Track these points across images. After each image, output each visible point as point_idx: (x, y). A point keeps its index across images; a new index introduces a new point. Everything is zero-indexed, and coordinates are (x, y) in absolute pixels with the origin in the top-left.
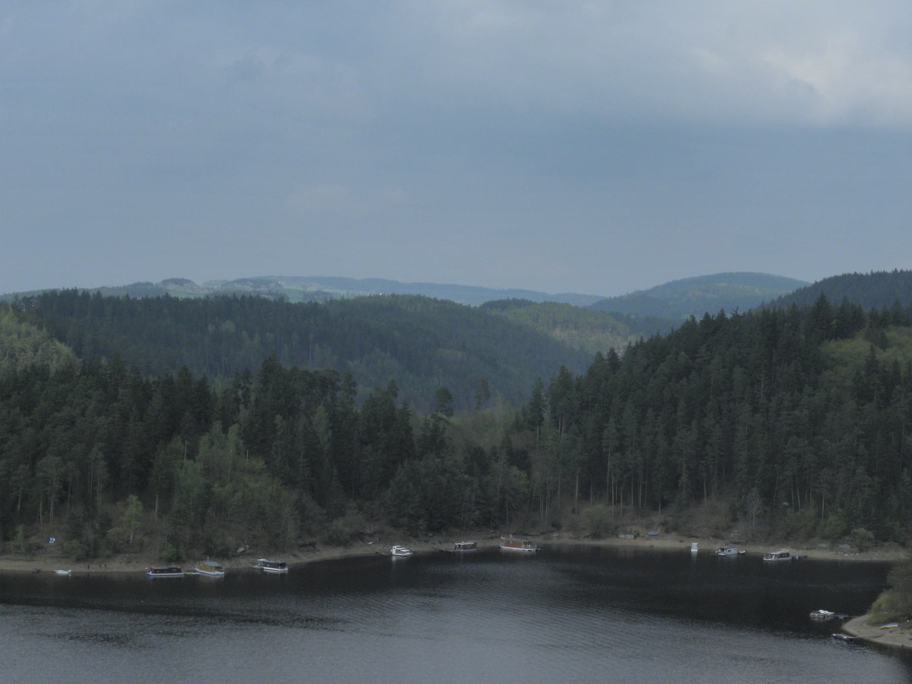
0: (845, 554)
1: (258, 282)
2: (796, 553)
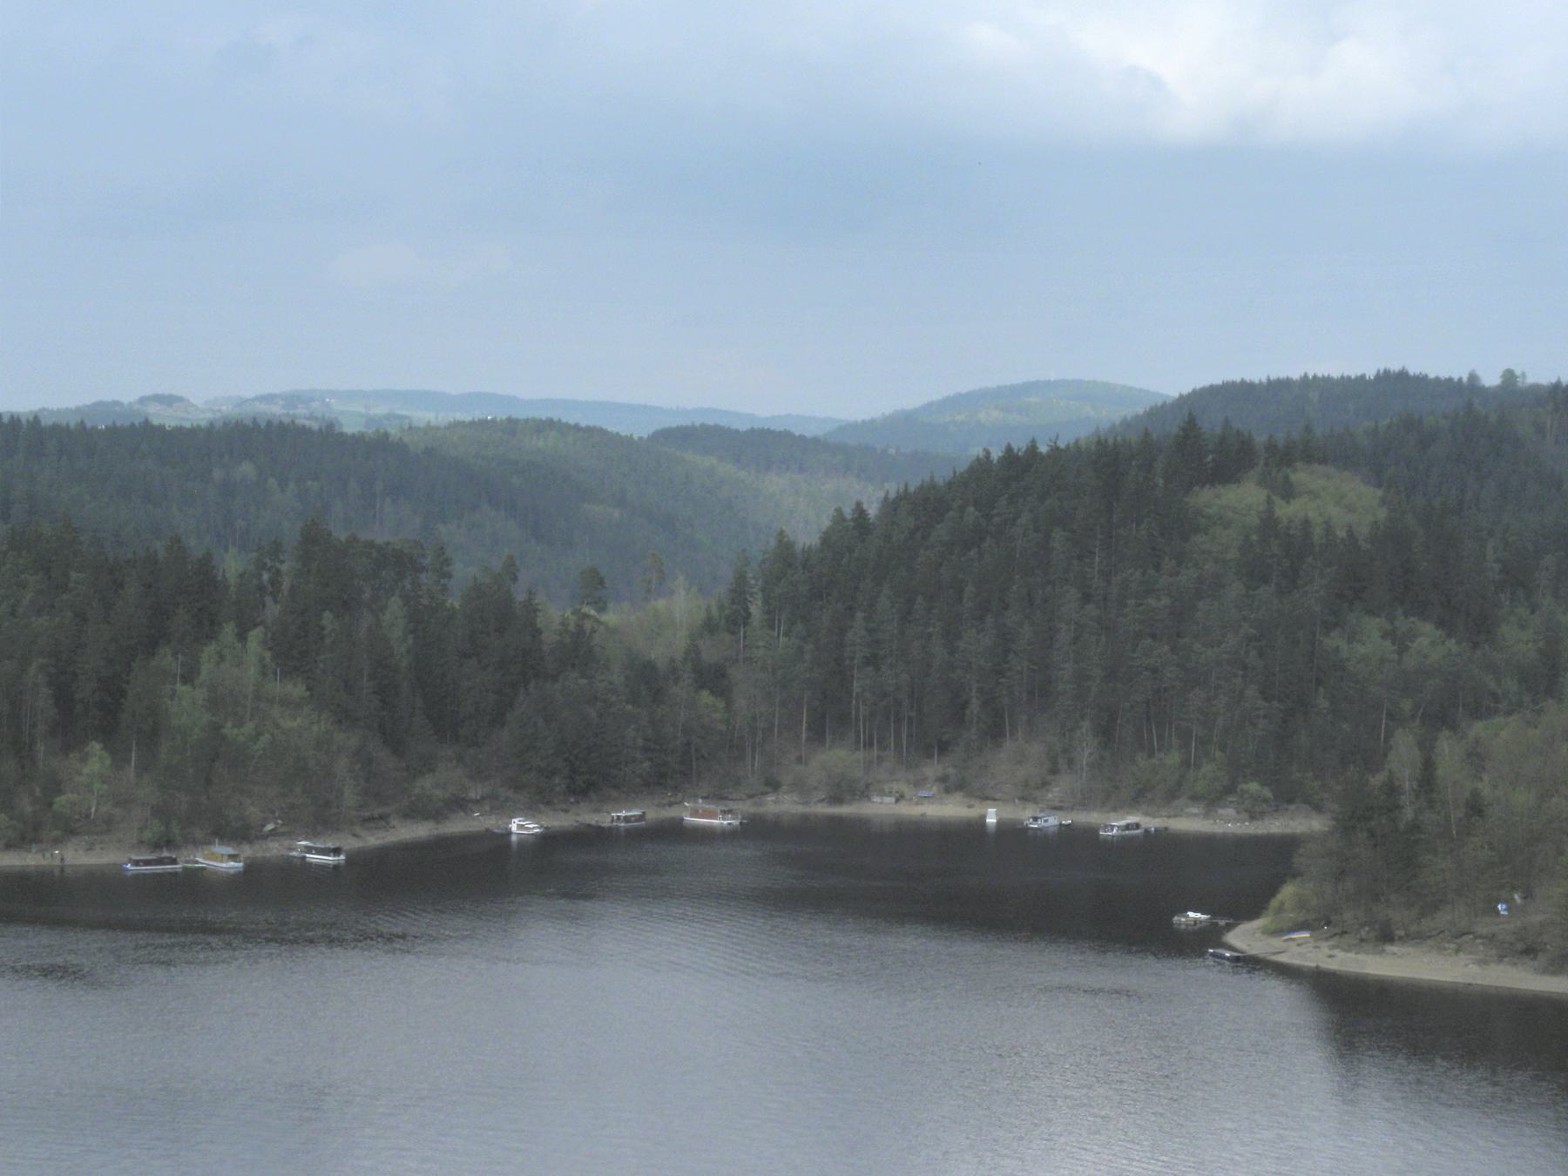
0: (1227, 823)
2: (1151, 823)
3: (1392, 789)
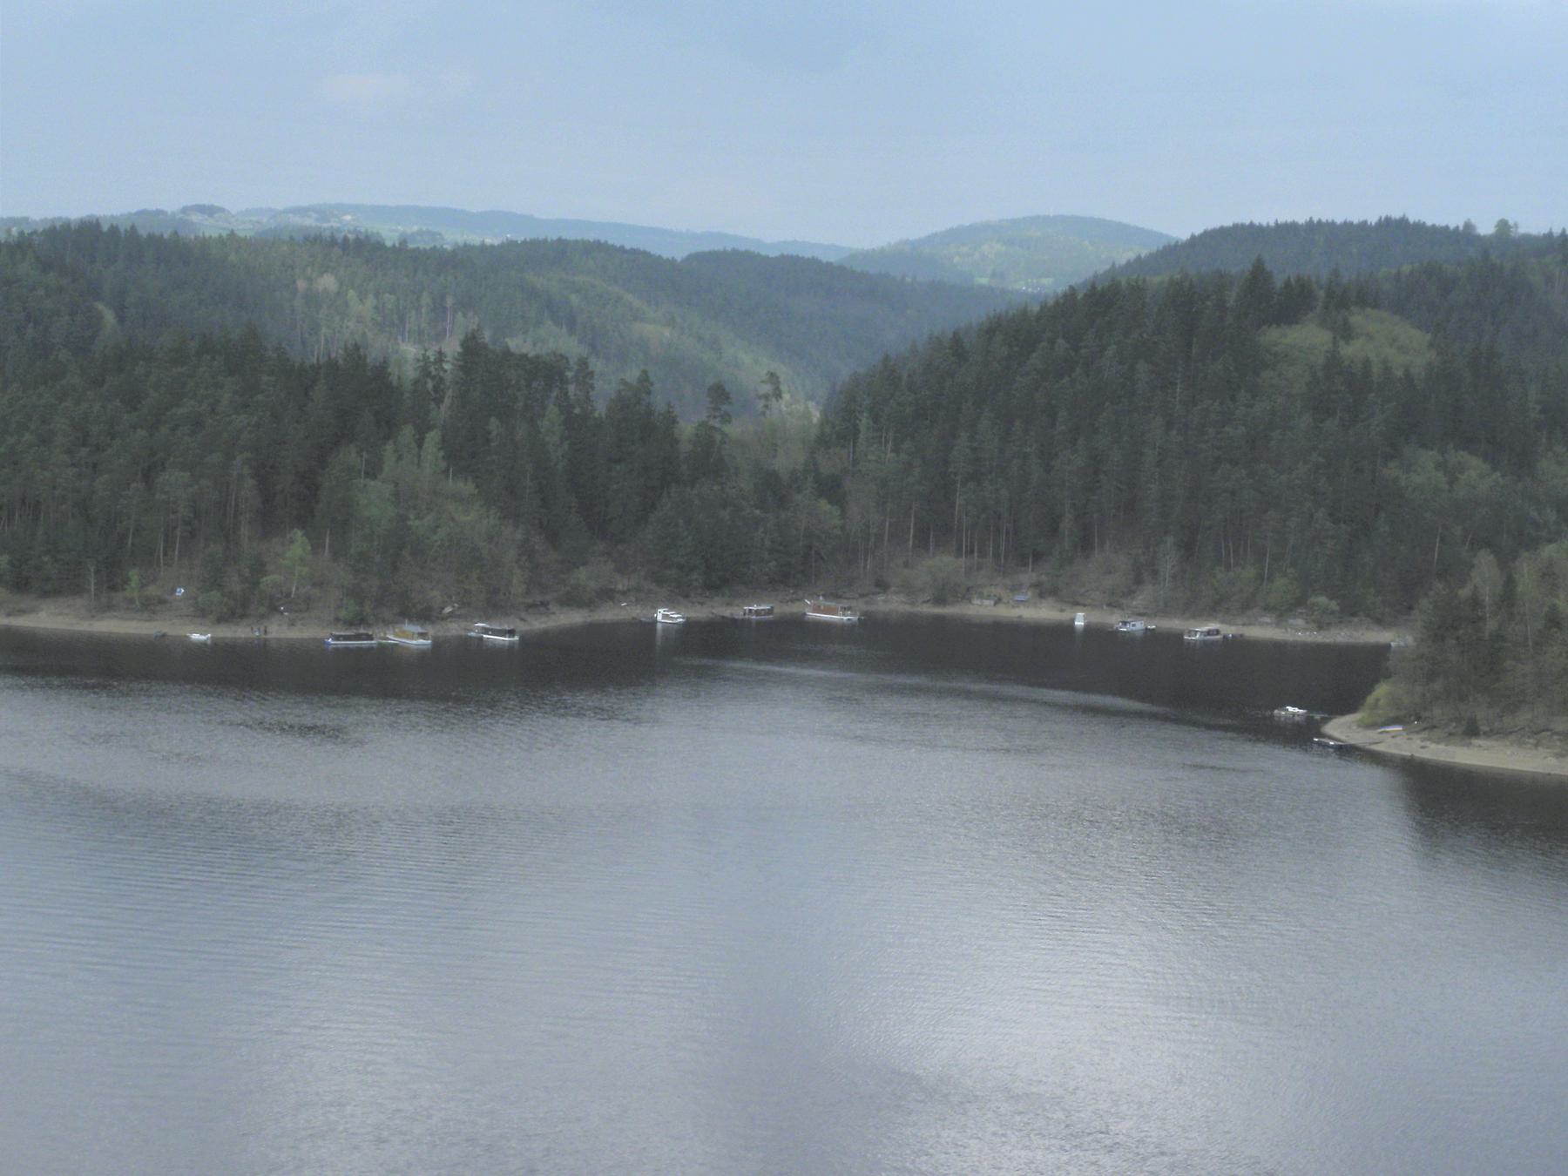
0: (1298, 632)
1: (323, 212)
2: (1230, 630)
3: (1476, 602)
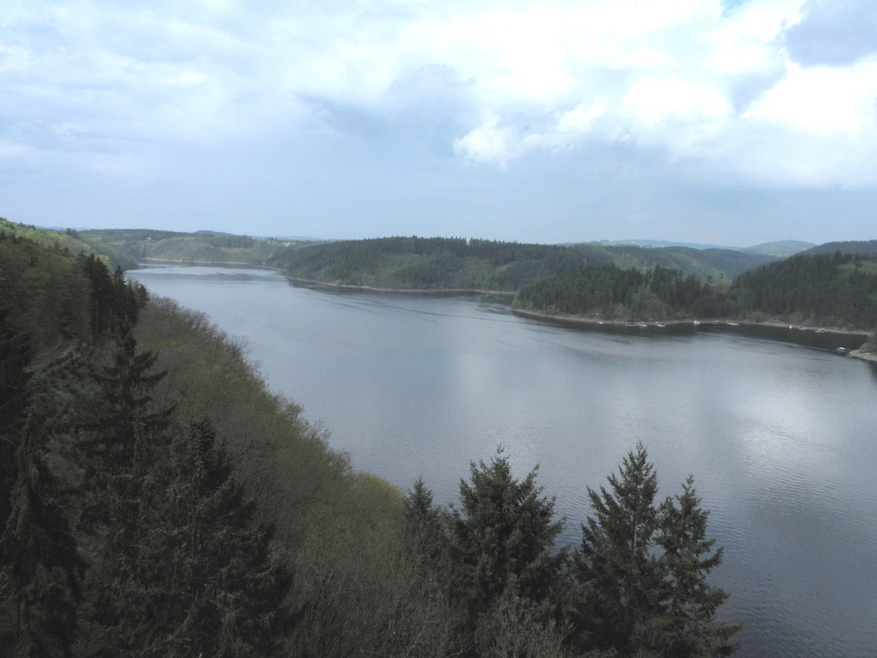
0: (844, 331)
2: (827, 330)
